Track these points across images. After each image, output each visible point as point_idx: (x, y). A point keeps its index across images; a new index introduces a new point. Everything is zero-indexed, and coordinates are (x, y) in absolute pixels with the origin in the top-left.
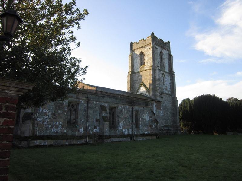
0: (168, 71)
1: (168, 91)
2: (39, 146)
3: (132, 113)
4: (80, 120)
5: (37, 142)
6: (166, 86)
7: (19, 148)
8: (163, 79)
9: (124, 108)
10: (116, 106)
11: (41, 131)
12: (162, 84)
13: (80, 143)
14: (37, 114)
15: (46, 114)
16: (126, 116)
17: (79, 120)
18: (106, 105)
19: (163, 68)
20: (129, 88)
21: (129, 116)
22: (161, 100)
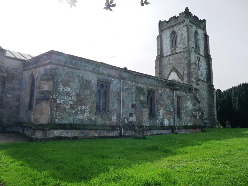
0: (204, 54)
1: (204, 78)
2: (59, 138)
3: (173, 99)
4: (113, 105)
5: (57, 133)
6: (202, 72)
7: (31, 140)
8: (199, 63)
9: (165, 92)
10: (155, 88)
11: (62, 117)
12: (198, 69)
13: (113, 135)
14: (56, 94)
15: (68, 94)
16: (166, 103)
17: (111, 106)
18: (144, 87)
19: (198, 50)
20: (158, 74)
21: (170, 103)
22: (198, 87)
